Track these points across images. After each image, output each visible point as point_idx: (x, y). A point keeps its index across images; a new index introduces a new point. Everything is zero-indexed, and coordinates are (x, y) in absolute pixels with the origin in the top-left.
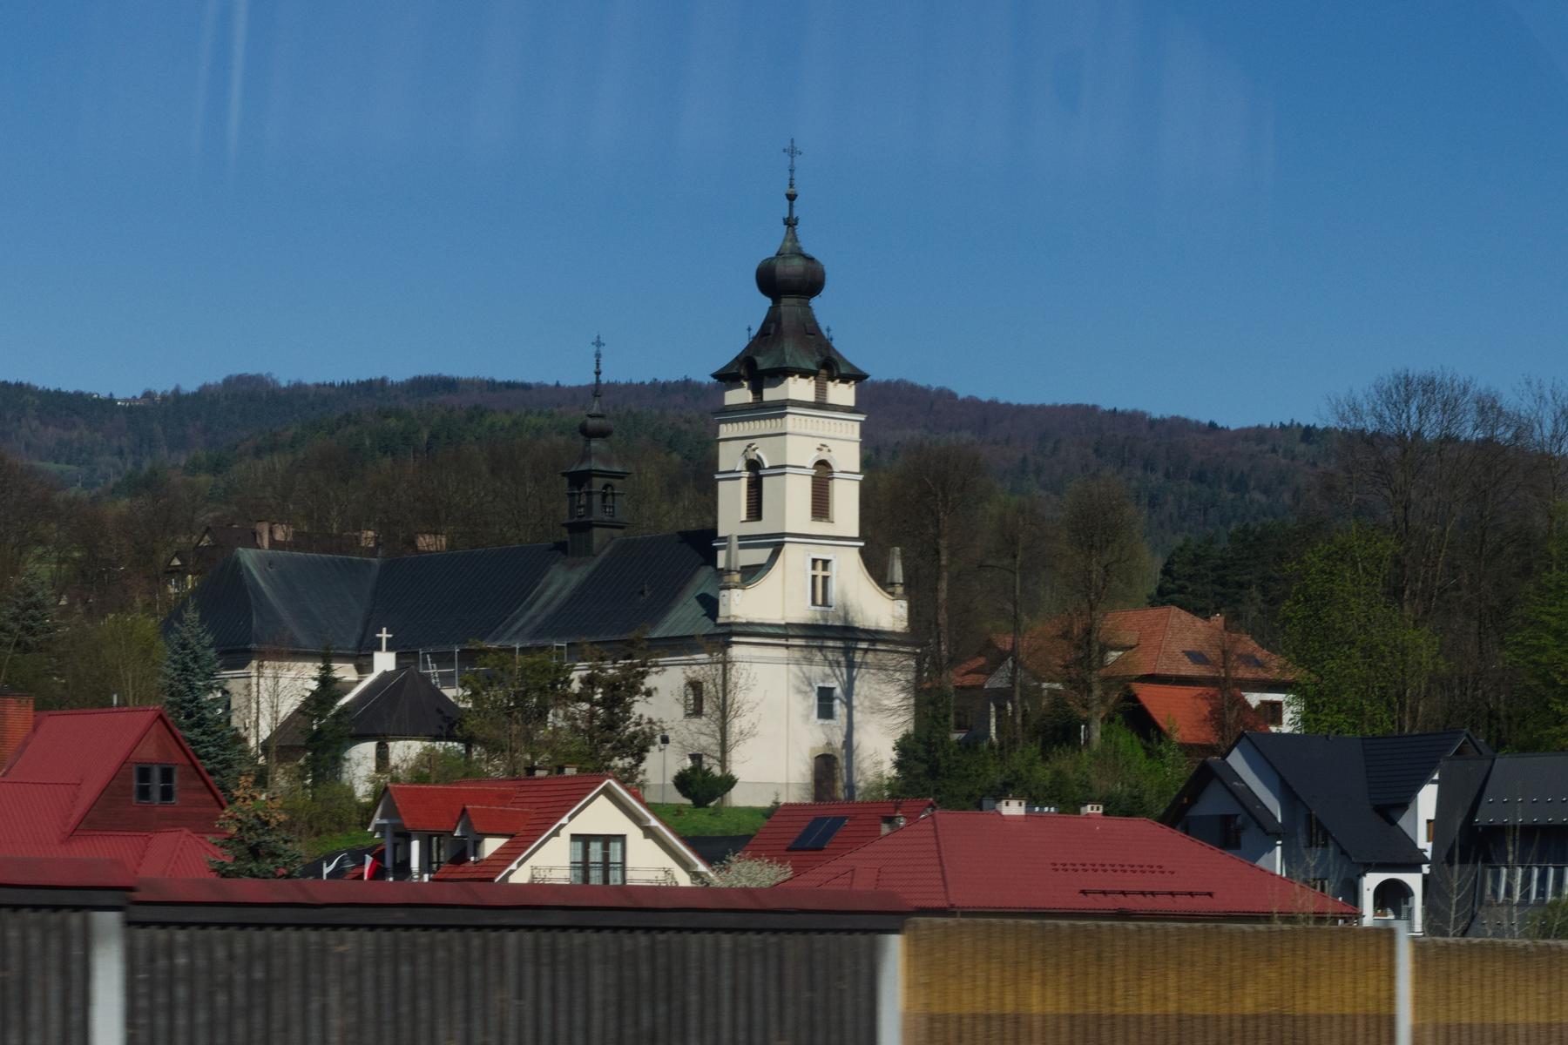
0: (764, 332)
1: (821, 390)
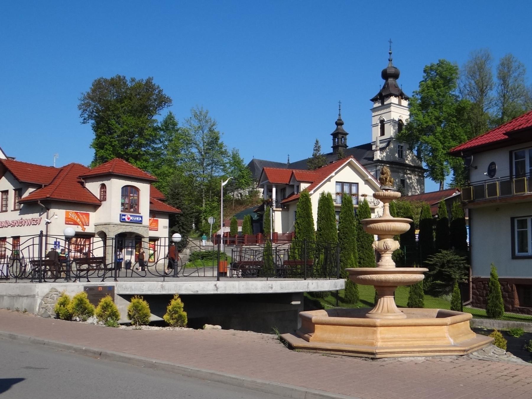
0: (384, 87)
1: (400, 102)
